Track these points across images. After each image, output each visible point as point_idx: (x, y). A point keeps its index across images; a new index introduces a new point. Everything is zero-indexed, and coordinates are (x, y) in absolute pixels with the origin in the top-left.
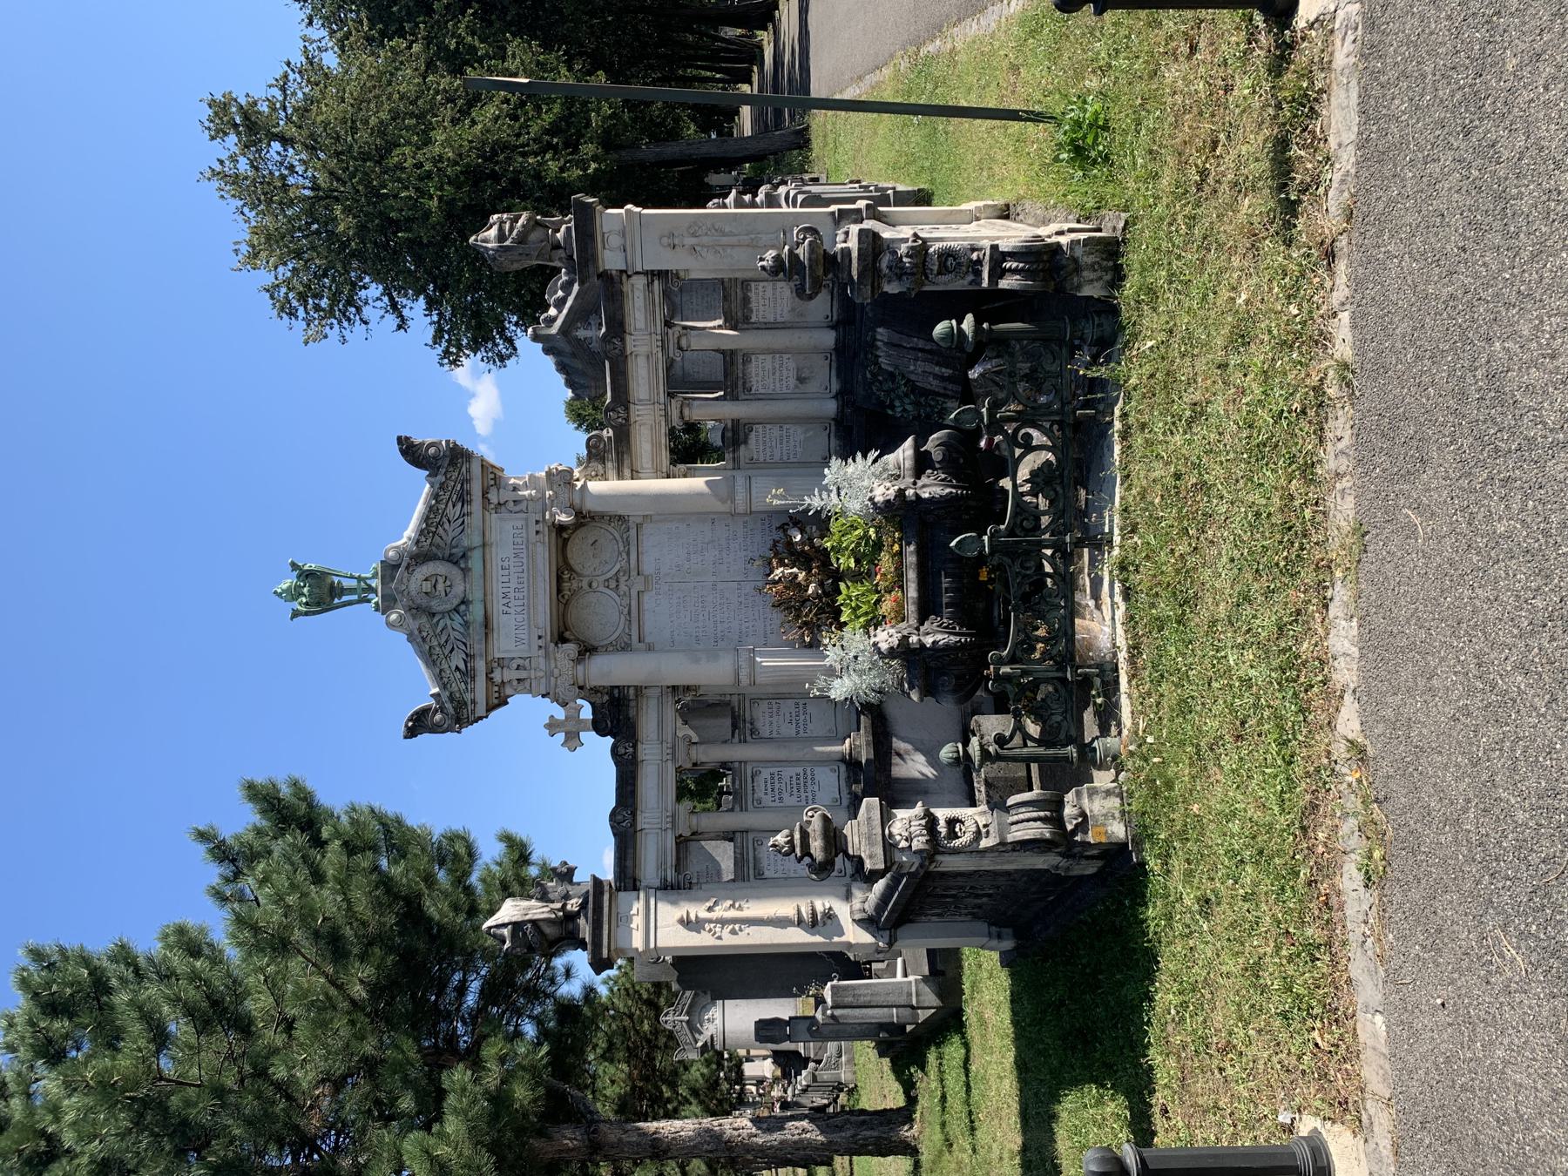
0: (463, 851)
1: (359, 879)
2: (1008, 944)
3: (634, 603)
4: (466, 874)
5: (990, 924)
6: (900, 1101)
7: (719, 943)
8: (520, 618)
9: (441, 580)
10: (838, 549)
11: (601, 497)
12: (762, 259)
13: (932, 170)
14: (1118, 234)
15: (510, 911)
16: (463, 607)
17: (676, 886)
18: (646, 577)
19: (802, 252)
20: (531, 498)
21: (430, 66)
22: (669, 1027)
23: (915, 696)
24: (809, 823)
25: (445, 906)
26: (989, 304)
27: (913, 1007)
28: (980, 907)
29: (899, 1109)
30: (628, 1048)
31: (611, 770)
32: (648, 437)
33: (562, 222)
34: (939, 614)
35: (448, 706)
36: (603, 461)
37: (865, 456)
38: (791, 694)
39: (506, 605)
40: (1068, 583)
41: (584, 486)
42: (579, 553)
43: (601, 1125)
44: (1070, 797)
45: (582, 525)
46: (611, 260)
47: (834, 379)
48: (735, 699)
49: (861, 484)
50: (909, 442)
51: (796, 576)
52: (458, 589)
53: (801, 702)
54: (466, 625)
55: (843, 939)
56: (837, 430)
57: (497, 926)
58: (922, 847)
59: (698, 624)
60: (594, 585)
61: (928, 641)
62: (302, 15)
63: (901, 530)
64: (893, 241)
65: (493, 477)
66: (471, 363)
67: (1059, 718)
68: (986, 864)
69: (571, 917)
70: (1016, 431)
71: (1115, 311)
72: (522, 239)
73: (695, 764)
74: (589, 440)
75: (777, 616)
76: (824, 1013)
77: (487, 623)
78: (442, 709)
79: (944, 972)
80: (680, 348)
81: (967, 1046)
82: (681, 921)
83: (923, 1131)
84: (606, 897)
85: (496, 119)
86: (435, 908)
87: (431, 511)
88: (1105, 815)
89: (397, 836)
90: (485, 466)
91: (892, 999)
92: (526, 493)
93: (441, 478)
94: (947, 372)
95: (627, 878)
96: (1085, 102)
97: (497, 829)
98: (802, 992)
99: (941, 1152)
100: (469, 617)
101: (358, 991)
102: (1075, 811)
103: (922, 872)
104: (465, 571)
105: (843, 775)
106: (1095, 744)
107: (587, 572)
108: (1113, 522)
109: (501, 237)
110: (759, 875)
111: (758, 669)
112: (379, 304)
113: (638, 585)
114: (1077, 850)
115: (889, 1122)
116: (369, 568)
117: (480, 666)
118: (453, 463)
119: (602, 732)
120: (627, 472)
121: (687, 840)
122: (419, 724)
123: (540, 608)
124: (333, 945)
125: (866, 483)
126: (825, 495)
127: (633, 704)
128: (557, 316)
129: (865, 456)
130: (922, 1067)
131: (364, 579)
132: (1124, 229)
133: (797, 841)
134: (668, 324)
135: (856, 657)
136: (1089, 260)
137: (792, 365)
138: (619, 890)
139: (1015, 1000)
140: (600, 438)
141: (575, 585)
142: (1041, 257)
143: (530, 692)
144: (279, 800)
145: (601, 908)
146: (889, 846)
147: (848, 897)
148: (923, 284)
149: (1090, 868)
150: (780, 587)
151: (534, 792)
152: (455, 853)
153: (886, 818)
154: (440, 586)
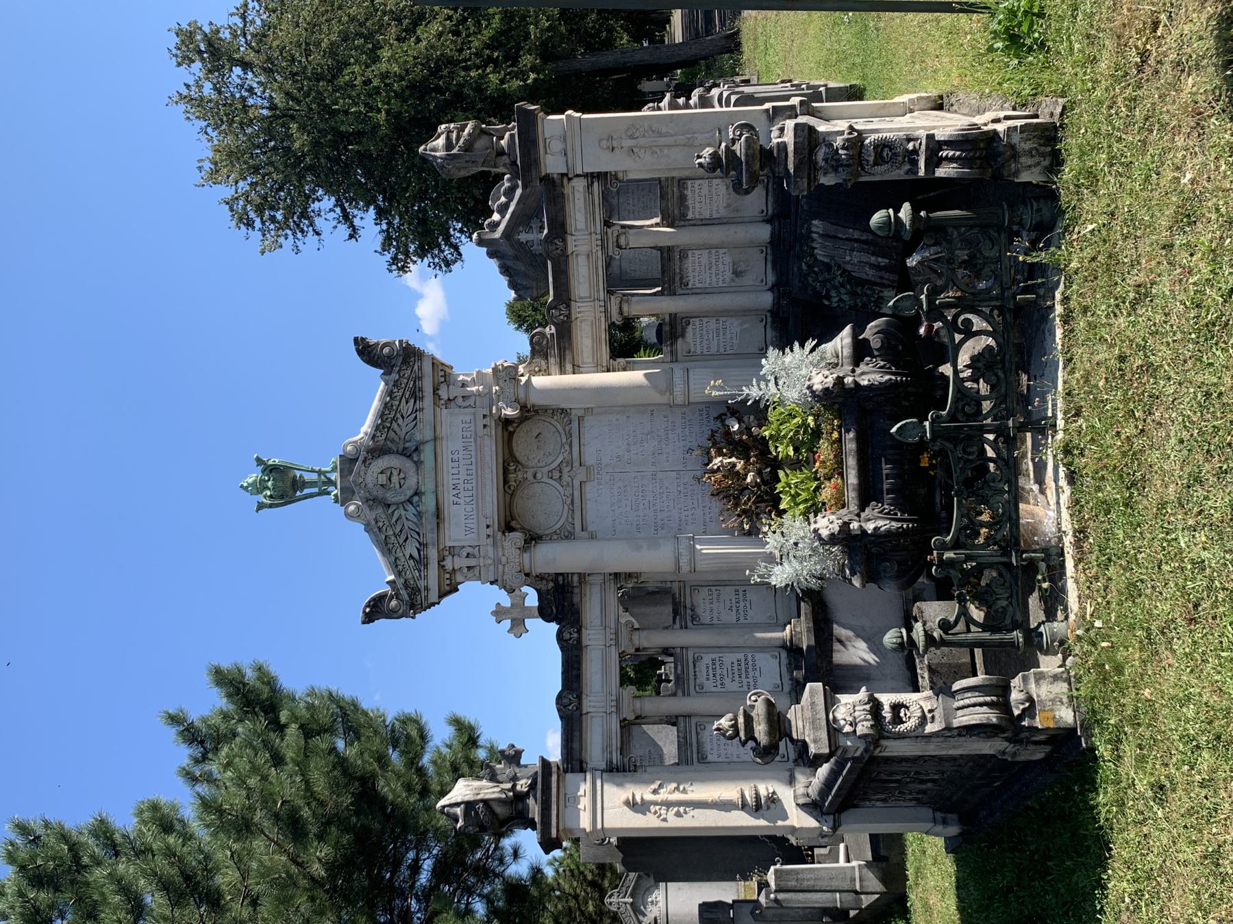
0: (414, 733)
2: (953, 830)
4: (419, 756)
5: (935, 810)
7: (664, 825)
8: (469, 508)
9: (395, 473)
10: (776, 438)
12: (699, 157)
13: (863, 65)
14: (1056, 119)
15: (463, 790)
16: (416, 499)
17: (622, 768)
18: (588, 468)
19: (739, 148)
20: (479, 394)
22: (613, 908)
23: (856, 582)
24: (753, 707)
26: (927, 193)
27: (856, 892)
28: (924, 792)
32: (589, 332)
34: (880, 500)
35: (403, 592)
37: (802, 346)
38: (732, 581)
40: (1011, 467)
44: (1016, 682)
45: (527, 418)
46: (552, 164)
47: (769, 271)
48: (676, 586)
49: (799, 374)
50: (847, 330)
51: (734, 465)
52: (412, 481)
53: (741, 589)
54: (419, 515)
55: (787, 823)
56: (773, 322)
57: (451, 805)
58: (866, 731)
59: (640, 510)
60: (539, 476)
61: (870, 527)
63: (840, 418)
65: (443, 373)
66: (418, 268)
67: (1004, 603)
68: (932, 749)
69: (520, 798)
70: (956, 317)
72: (468, 147)
73: (637, 650)
75: (716, 505)
76: (767, 897)
77: (438, 514)
79: (888, 858)
80: (619, 247)
82: (627, 803)
84: (554, 778)
85: (440, 35)
86: (389, 788)
88: (1053, 700)
89: (348, 717)
90: (435, 363)
91: (835, 884)
92: (474, 389)
93: (395, 376)
94: (883, 261)
95: (574, 760)
97: (446, 713)
98: (746, 878)
101: (317, 870)
102: (1022, 696)
104: (418, 464)
105: (784, 660)
106: (1042, 629)
107: (531, 464)
108: (1056, 406)
109: (449, 145)
110: (702, 759)
113: (581, 475)
116: (328, 462)
117: (433, 554)
118: (405, 361)
120: (569, 367)
121: (631, 723)
122: (376, 610)
123: (488, 499)
124: (293, 826)
125: (804, 372)
127: (576, 591)
128: (500, 220)
129: (802, 346)
131: (324, 473)
132: (1062, 114)
134: (607, 224)
135: (796, 544)
136: (1027, 146)
137: (728, 259)
138: (566, 771)
140: (542, 335)
142: (977, 145)
143: (479, 579)
144: (244, 685)
145: (550, 788)
146: (833, 730)
147: (791, 781)
149: (1038, 754)
150: (719, 476)
152: (408, 736)
153: (830, 703)
154: (395, 479)
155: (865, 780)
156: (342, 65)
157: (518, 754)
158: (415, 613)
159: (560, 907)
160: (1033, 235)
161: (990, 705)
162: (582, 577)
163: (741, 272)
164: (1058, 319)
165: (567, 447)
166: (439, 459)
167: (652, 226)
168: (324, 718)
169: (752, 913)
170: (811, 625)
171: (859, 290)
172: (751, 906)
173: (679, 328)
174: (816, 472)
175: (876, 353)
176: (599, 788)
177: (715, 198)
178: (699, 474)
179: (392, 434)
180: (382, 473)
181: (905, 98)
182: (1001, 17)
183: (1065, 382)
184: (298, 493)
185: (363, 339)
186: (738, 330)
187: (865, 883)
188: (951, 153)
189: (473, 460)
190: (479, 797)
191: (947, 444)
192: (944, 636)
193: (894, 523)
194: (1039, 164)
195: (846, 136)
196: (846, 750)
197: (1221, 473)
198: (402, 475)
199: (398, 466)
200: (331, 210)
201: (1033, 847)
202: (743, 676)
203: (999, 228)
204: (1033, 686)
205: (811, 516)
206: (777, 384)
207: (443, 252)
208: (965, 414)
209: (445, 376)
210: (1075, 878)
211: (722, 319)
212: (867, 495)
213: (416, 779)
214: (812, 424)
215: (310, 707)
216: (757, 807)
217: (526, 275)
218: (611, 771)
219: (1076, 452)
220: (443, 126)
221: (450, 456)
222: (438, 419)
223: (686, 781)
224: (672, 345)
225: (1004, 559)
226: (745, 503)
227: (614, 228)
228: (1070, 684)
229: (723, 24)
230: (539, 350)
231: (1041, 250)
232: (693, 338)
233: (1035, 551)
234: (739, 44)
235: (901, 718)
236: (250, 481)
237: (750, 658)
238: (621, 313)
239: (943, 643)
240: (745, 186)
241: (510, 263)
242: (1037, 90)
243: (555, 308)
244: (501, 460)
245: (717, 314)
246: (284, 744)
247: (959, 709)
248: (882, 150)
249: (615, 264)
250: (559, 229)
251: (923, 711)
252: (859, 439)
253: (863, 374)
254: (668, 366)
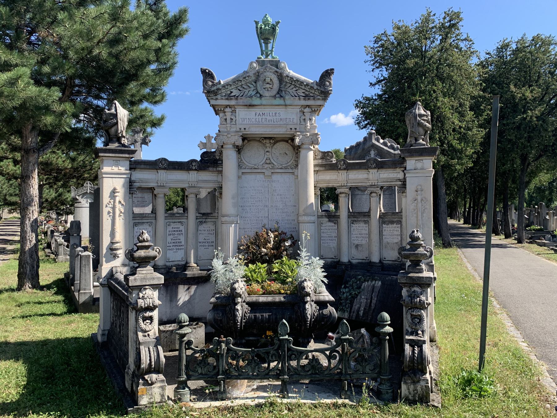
0: (157, 99)
1: (144, 53)
2: (100, 339)
4: (147, 100)
5: (109, 330)
6: (42, 283)
7: (104, 206)
8: (253, 120)
9: (271, 86)
10: (282, 263)
11: (306, 157)
12: (417, 231)
13: (444, 303)
14: (431, 403)
15: (123, 114)
16: (258, 95)
17: (131, 187)
18: (271, 176)
19: (421, 250)
20: (306, 127)
21: (473, 98)
22: (85, 185)
23: (213, 300)
24: (153, 250)
25: (134, 91)
26: (397, 340)
27: (79, 291)
28: (116, 326)
29: (39, 283)
30: (78, 168)
31: (186, 159)
32: (333, 178)
33: (427, 142)
34: (251, 312)
35: (215, 88)
36: (322, 158)
37: (325, 277)
38: (217, 241)
39: (259, 114)
40: (266, 375)
41: (311, 150)
42: (282, 147)
43: (37, 154)
44: (161, 377)
45: (294, 149)
46: (411, 163)
47: (357, 261)
48: (216, 214)
49: (311, 274)
50: (332, 299)
51: (270, 243)
52: (266, 94)
53: (214, 244)
54: (251, 97)
55: (104, 263)
56: (334, 262)
57: (116, 107)
58: (139, 304)
59: (251, 200)
60: (268, 153)
63: (291, 294)
64: (427, 293)
65: (315, 110)
66: (357, 112)
67: (200, 372)
68: (131, 335)
69: (119, 140)
70: (338, 352)
71: (394, 401)
72: (420, 124)
73: (187, 196)
74: (331, 152)
75: (252, 234)
76: (80, 251)
77: (251, 106)
78: (214, 85)
79: (92, 305)
80: (371, 193)
81: (61, 315)
82: (115, 189)
83: (29, 293)
84: (127, 156)
85: (453, 123)
86: (133, 86)
87: (302, 83)
88: (152, 394)
89: (165, 70)
91: (83, 282)
92: (308, 124)
93: (315, 87)
94: (361, 313)
95: (135, 165)
96: (491, 385)
97: (167, 115)
98: (90, 241)
99: (16, 301)
100: (254, 98)
101: (96, 52)
102: (154, 380)
103: (128, 303)
104: (275, 97)
105: (180, 263)
106: (187, 389)
107: (273, 150)
108: (293, 399)
109: (421, 116)
110: (135, 225)
111: (228, 225)
112: (380, 75)
113: (268, 173)
114: (136, 379)
115: (33, 278)
116: (276, 56)
117: (233, 102)
118: (322, 92)
119: (203, 155)
120: (317, 169)
121: (153, 192)
122: (207, 75)
124: (115, 41)
125: (313, 277)
126: (307, 258)
127: (215, 169)
129: (325, 277)
130: (56, 293)
131: (272, 53)
132: (433, 406)
133: (144, 244)
134: (382, 188)
135: (232, 271)
136: (419, 388)
137: (364, 242)
138: (130, 161)
140: (332, 157)
142: (419, 366)
143: (221, 124)
144: (180, 23)
146: (140, 288)
147: (124, 265)
148: (406, 307)
149: (128, 385)
150: (265, 236)
151: (181, 127)
152: (155, 97)
153: (154, 287)
154: (268, 86)
155: (120, 298)
156: (442, 80)
157: (146, 144)
158: (205, 93)
159: (87, 162)
160: (376, 388)
161: (150, 364)
162: (221, 172)
163: (357, 248)
164: (335, 401)
165: (280, 167)
166: (277, 107)
167: (380, 208)
168: (163, 59)
169: (75, 244)
170: (196, 276)
171: (348, 301)
172: (78, 243)
173: (333, 219)
174: (266, 282)
175: (321, 312)
176: (122, 176)
177: (392, 237)
178: (267, 227)
180: (271, 80)
181: (435, 325)
182: (479, 376)
183: (305, 404)
184: (262, 41)
185: (333, 73)
186: (332, 246)
187: (83, 295)
188: (416, 352)
189: (276, 123)
190: (119, 120)
191: (277, 346)
192: (185, 342)
193: (240, 318)
194: (410, 393)
195: (426, 302)
196: (131, 293)
198: (269, 89)
199: (274, 87)
200: (382, 75)
201: (87, 378)
202: (174, 244)
203: (379, 373)
204: (159, 385)
205: (245, 279)
206: (307, 265)
207: (364, 122)
208: (291, 355)
209: (315, 111)
210: (68, 400)
211: (336, 239)
212: (254, 306)
213: (137, 98)
214: (288, 280)
215: (169, 53)
216: (112, 249)
217: (355, 154)
218: (130, 182)
219: (271, 408)
220: (429, 113)
221: (278, 112)
222: (295, 107)
223: (125, 217)
224: (326, 216)
225: (221, 372)
226: (252, 247)
227: (380, 191)
228: (159, 403)
229: (454, 240)
230: (325, 155)
231: (369, 394)
232: (328, 225)
233: (224, 386)
234: (446, 247)
235: (145, 320)
236: (269, 19)
237: (182, 247)
238: (341, 193)
239: (181, 342)
240: (403, 253)
241: (361, 146)
242: (445, 393)
243: (344, 163)
244: (275, 136)
245: (339, 237)
246: (153, 40)
247: (149, 349)
248: (418, 318)
249: (359, 192)
250: (380, 166)
251: (149, 331)
252: (280, 303)
253: (311, 305)
254: (316, 214)
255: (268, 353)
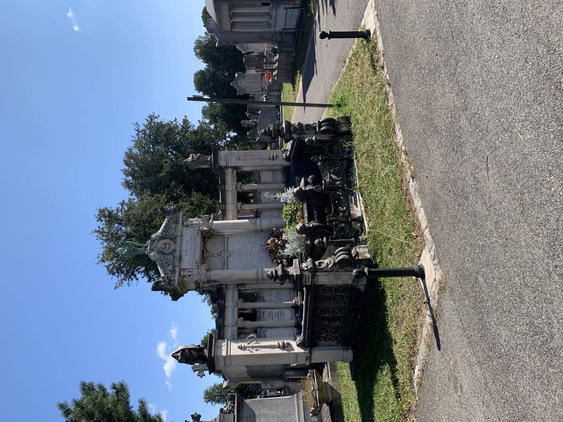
3: (226, 262)
20: (196, 224)
34: (314, 220)
52: (173, 247)
61: (311, 226)
62: (130, 193)
77: (180, 257)
78: (164, 281)
84: (214, 340)
109: (193, 158)
117: (177, 269)
123: (197, 254)
136: (343, 121)
139: (358, 395)
141: (208, 255)
145: (212, 342)
147: (295, 339)
154: (167, 246)
179: (168, 233)
197: (487, 418)
212: (310, 219)
216: (284, 347)
252: (307, 205)
255: (333, 196)
